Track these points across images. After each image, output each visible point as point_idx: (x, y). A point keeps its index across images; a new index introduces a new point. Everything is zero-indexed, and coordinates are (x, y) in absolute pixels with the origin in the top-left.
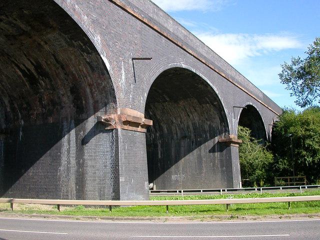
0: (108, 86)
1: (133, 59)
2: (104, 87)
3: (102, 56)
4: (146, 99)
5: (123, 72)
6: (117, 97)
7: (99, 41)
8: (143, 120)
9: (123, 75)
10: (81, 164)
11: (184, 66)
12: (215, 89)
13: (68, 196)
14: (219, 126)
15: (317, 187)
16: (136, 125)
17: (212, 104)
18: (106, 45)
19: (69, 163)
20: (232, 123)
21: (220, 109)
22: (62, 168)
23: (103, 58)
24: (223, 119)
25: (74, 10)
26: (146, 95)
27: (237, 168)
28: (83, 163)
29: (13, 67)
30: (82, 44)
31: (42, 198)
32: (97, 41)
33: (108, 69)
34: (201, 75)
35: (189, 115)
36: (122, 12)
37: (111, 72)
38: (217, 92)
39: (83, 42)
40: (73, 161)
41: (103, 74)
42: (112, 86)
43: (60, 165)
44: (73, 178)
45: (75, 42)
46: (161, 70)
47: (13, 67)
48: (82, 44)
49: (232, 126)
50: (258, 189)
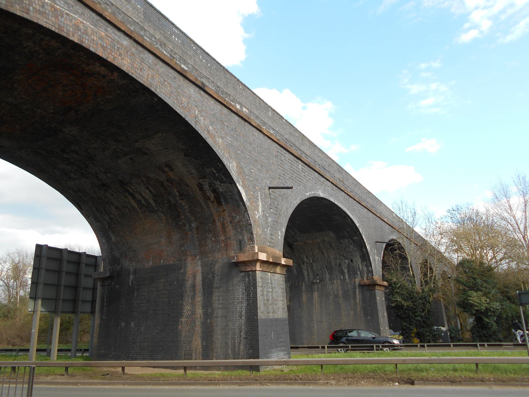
0: (244, 220)
1: (270, 188)
2: (239, 222)
3: (238, 185)
4: (284, 235)
5: (260, 204)
6: (254, 232)
7: (235, 168)
8: (283, 261)
9: (260, 206)
10: (208, 315)
11: (322, 195)
12: (356, 222)
13: (191, 355)
14: (360, 265)
15: (501, 345)
16: (276, 264)
17: (351, 239)
18: (241, 172)
19: (194, 313)
20: (375, 262)
21: (362, 245)
22: (184, 320)
23: (239, 187)
24: (365, 257)
25: (208, 132)
26: (284, 230)
27: (383, 317)
28: (212, 313)
29: (126, 197)
30: (215, 171)
31: (157, 359)
32: (232, 167)
33: (245, 200)
34: (340, 205)
35: (323, 253)
36: (257, 133)
37: (247, 204)
38: (358, 225)
39: (216, 170)
40: (199, 311)
41: (238, 206)
42: (248, 220)
43: (182, 316)
44: (198, 329)
45: (208, 168)
46: (298, 201)
47: (126, 197)
48: (215, 171)
49: (375, 265)
50: (421, 346)
